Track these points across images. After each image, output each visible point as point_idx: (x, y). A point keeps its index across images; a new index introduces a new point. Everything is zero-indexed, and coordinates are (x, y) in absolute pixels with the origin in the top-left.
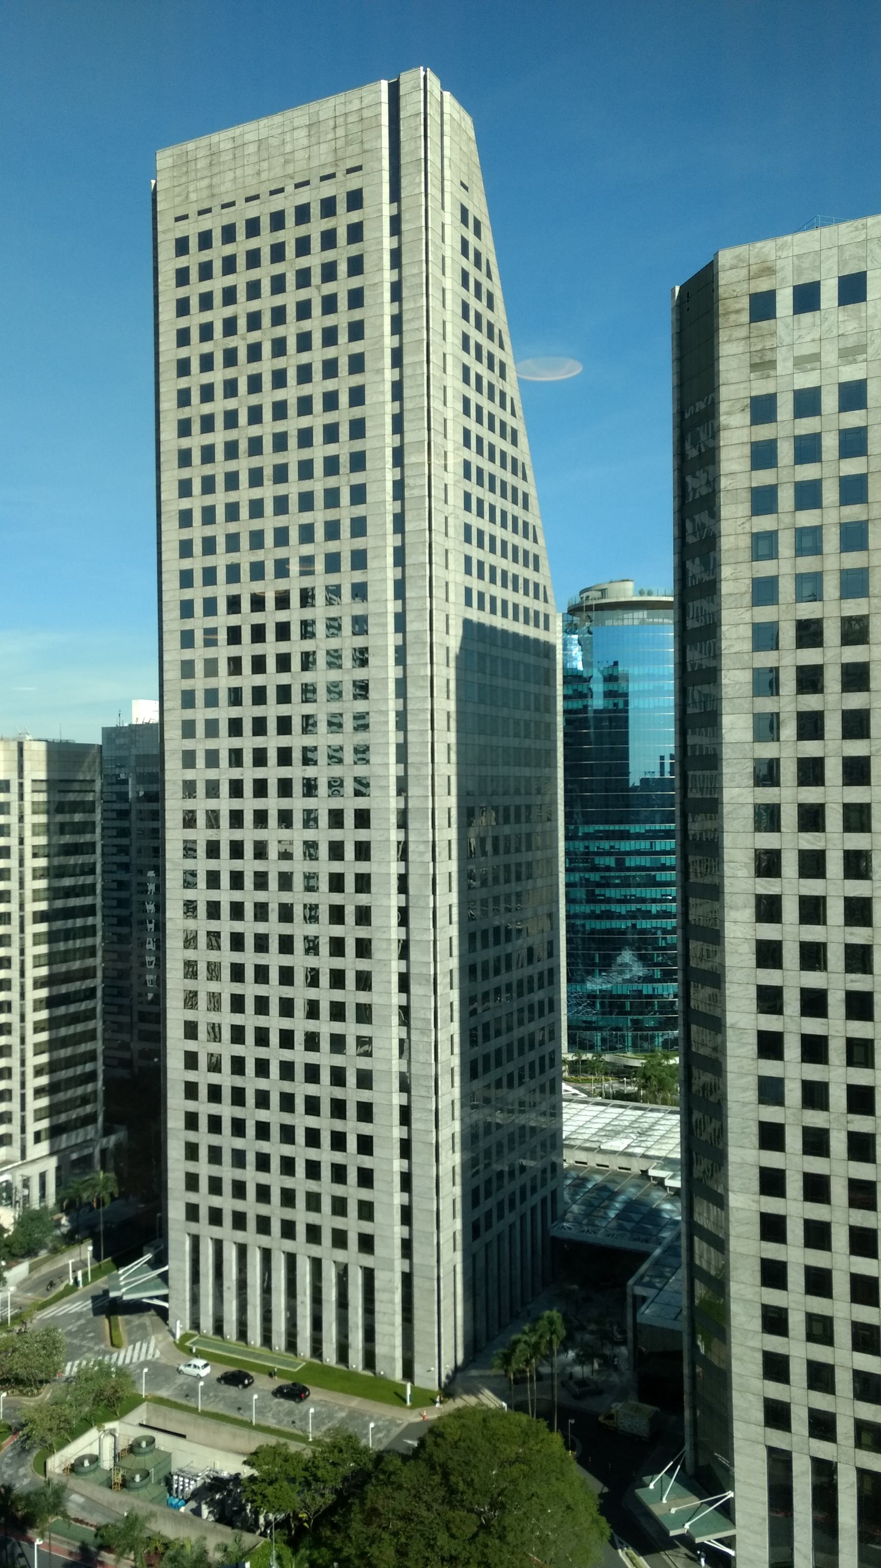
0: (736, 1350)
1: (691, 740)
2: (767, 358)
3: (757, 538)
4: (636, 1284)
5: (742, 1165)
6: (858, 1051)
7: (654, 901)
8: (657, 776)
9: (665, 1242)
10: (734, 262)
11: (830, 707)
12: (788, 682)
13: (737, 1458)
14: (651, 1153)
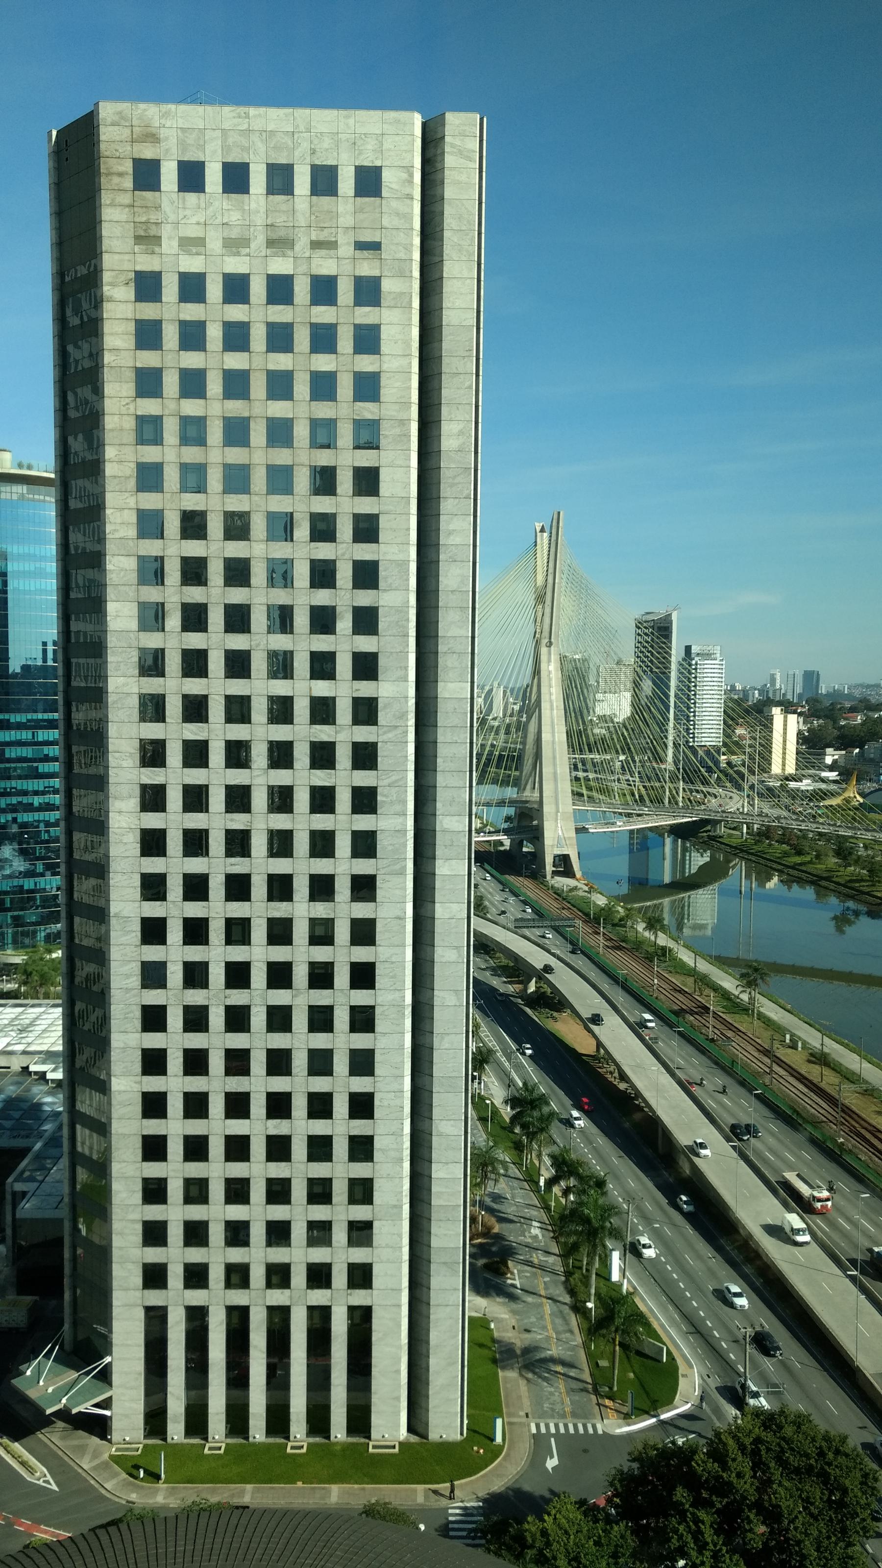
0: (116, 1225)
1: (74, 626)
2: (152, 233)
3: (142, 420)
4: (15, 1180)
5: (124, 1049)
6: (236, 931)
7: (36, 793)
8: (40, 663)
9: (47, 1134)
10: (116, 118)
11: (213, 600)
12: (173, 572)
13: (115, 1324)
14: (32, 1048)
